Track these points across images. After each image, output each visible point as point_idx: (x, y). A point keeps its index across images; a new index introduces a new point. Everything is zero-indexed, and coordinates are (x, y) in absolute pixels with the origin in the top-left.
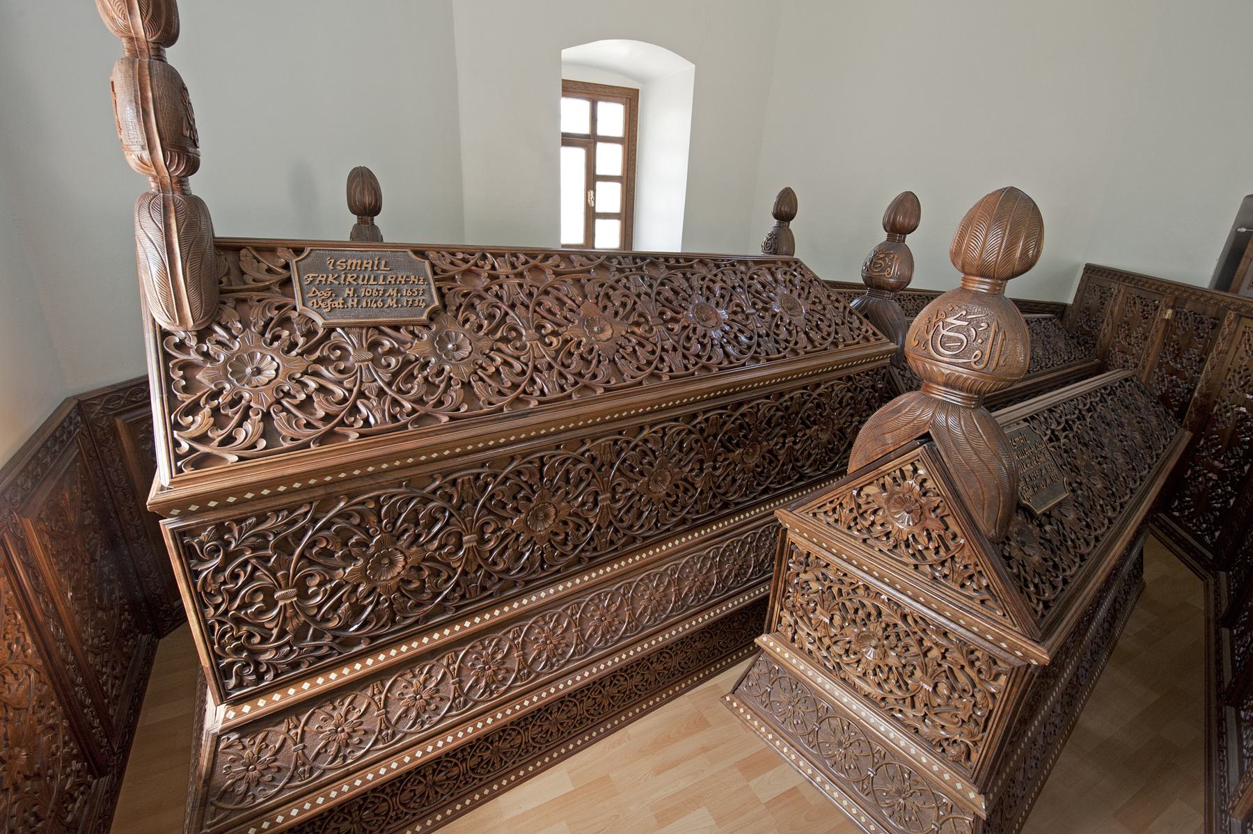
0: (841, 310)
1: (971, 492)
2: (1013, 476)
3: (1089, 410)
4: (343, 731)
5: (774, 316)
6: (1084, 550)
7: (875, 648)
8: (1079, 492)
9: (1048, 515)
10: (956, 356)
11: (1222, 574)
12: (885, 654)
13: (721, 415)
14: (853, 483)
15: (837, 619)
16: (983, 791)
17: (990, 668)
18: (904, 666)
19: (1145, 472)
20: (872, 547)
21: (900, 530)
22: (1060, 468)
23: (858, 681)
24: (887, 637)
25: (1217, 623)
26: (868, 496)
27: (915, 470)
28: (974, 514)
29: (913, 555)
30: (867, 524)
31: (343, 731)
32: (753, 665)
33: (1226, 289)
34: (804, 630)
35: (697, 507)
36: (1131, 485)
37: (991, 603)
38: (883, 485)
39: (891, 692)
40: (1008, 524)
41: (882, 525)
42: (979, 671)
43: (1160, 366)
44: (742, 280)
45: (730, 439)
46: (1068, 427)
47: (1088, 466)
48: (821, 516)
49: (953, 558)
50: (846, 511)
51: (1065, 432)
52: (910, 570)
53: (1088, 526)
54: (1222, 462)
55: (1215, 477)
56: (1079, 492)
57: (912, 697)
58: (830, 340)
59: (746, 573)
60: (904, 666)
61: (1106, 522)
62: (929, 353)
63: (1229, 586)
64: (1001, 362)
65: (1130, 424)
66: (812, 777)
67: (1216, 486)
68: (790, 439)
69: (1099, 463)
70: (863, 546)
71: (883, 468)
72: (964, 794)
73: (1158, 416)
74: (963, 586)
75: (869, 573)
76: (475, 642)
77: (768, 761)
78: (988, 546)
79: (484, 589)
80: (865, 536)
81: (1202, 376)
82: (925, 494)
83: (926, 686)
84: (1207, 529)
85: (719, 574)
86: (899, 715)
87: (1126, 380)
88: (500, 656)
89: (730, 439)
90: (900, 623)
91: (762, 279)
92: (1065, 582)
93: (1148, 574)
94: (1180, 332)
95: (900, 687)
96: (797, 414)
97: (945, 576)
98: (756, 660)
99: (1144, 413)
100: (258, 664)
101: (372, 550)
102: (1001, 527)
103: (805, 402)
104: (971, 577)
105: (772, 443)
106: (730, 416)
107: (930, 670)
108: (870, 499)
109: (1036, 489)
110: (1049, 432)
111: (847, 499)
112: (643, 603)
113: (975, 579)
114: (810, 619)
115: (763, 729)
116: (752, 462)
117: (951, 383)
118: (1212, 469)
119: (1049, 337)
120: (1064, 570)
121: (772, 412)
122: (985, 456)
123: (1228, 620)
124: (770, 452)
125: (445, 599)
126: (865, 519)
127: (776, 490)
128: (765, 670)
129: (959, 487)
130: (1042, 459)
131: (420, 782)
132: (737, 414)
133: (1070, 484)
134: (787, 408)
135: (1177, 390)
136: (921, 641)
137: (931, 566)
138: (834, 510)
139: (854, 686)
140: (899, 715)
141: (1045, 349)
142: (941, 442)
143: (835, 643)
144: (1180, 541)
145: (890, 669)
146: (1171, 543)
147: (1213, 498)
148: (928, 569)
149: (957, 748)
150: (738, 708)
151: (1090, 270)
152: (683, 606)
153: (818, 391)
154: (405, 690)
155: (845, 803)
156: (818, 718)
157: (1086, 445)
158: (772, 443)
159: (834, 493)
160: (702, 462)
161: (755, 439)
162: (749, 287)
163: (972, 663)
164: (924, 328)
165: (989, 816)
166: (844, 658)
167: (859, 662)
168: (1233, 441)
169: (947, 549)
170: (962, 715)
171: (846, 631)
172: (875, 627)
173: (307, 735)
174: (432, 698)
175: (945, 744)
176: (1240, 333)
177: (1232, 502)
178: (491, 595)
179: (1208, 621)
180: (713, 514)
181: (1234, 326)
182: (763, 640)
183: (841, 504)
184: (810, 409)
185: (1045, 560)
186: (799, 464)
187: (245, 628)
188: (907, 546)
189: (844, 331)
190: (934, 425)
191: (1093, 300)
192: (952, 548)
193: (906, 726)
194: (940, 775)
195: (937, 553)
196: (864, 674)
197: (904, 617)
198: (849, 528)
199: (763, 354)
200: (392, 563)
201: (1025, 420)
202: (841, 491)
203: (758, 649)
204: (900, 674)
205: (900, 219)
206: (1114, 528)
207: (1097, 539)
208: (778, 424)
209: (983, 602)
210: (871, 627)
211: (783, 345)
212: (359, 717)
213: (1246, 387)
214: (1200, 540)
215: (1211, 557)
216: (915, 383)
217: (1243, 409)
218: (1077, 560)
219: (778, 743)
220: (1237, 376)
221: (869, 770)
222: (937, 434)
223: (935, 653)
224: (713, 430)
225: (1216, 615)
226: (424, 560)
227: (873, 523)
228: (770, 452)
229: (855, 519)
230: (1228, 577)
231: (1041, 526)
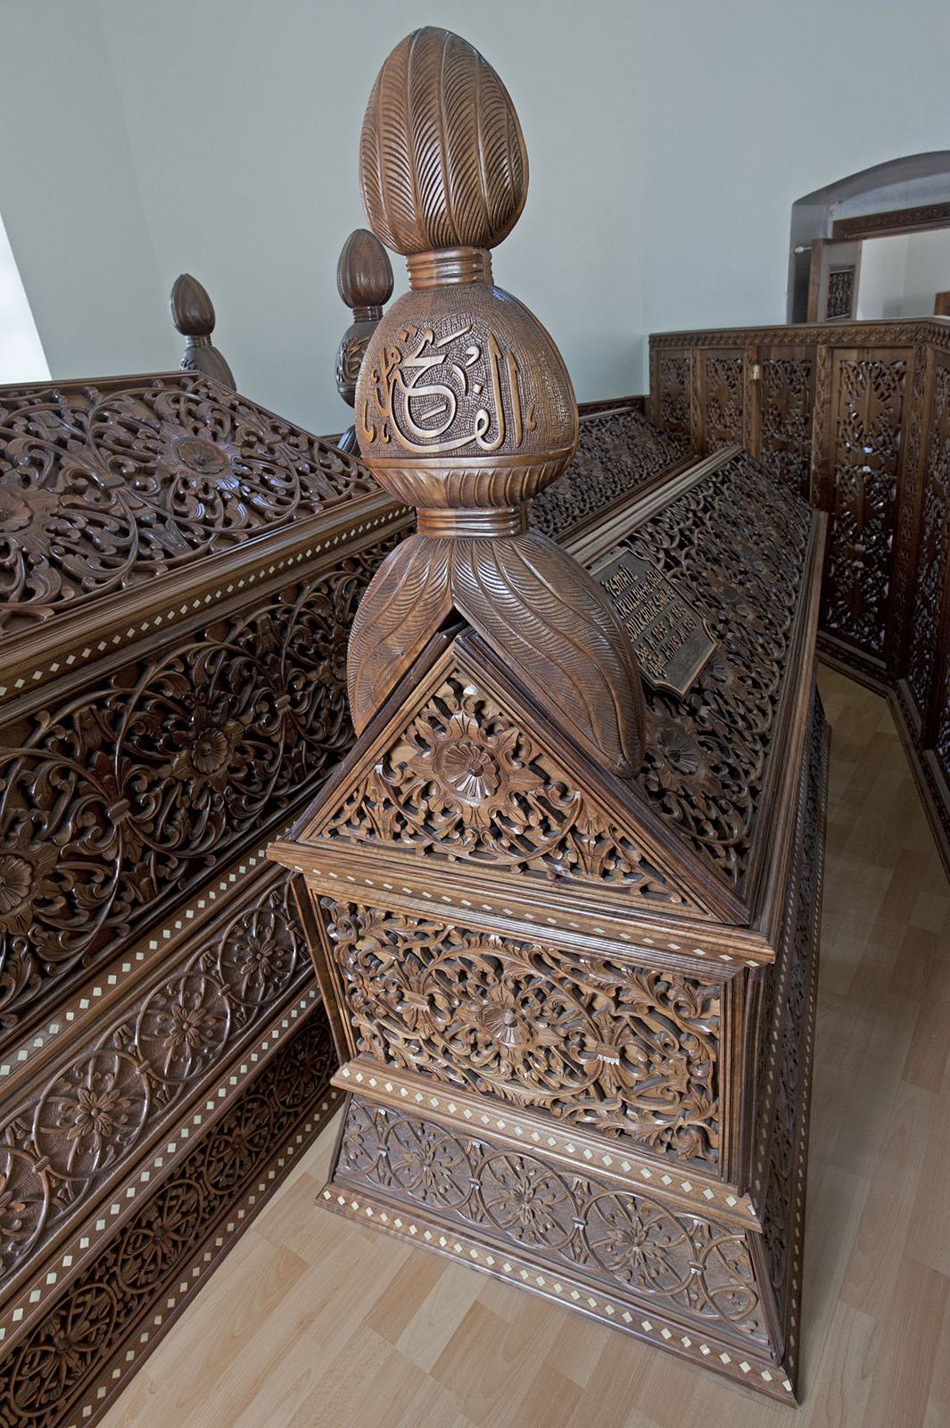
0: (304, 447)
1: (561, 699)
2: (620, 643)
3: (705, 510)
5: (168, 481)
6: (762, 726)
7: (513, 1025)
8: (729, 635)
9: (697, 690)
10: (445, 436)
11: (902, 682)
12: (532, 1032)
13: (100, 703)
14: (370, 753)
15: (441, 1002)
16: (744, 1189)
17: (691, 996)
18: (567, 1038)
19: (797, 579)
20: (444, 857)
21: (475, 812)
22: (692, 606)
23: (509, 1089)
24: (525, 1001)
25: (917, 747)
26: (402, 767)
27: (459, 690)
28: (578, 737)
29: (512, 848)
30: (419, 819)
32: (346, 1123)
33: (805, 321)
34: (398, 1037)
35: (130, 894)
36: (788, 603)
37: (657, 887)
38: (418, 737)
39: (562, 1086)
40: (640, 733)
41: (445, 811)
42: (678, 1007)
43: (766, 444)
44: (79, 425)
45: (148, 742)
46: (685, 542)
47: (729, 592)
48: (345, 831)
49: (573, 830)
50: (379, 807)
51: (684, 548)
52: (516, 876)
53: (756, 684)
54: (863, 543)
55: (860, 564)
56: (729, 635)
57: (596, 1084)
58: (296, 501)
59: (286, 964)
60: (567, 1038)
61: (776, 668)
62: (400, 447)
63: (914, 694)
64: (527, 421)
65: (760, 518)
66: (497, 1268)
67: (865, 575)
68: (281, 702)
69: (741, 583)
70: (429, 862)
71: (407, 706)
72: (718, 1203)
73: (785, 500)
74: (605, 873)
75: (456, 903)
77: (421, 1276)
78: (621, 788)
80: (427, 842)
81: (813, 441)
82: (490, 730)
83: (609, 1060)
84: (870, 633)
85: (232, 992)
86: (588, 1119)
87: (737, 459)
89: (148, 742)
90: (533, 972)
91: (126, 416)
92: (754, 792)
93: (831, 716)
94: (775, 393)
95: (572, 1074)
96: (277, 651)
97: (573, 867)
98: (347, 1113)
99: (770, 500)
102: (631, 746)
103: (284, 626)
104: (612, 854)
105: (247, 719)
106: (124, 698)
107: (605, 1032)
108: (408, 773)
109: (667, 652)
110: (661, 555)
111: (371, 787)
112: (73, 1137)
113: (619, 853)
114: (399, 1015)
115: (398, 1223)
116: (217, 767)
117: (461, 498)
118: (856, 556)
119: (632, 438)
120: (747, 773)
121: (221, 661)
122: (561, 622)
123: (928, 740)
124: (250, 735)
126: (415, 811)
127: (291, 797)
128: (366, 1123)
129: (539, 697)
130: (664, 600)
131: (146, 1237)
132: (140, 689)
133: (714, 628)
134: (251, 646)
135: (792, 468)
136: (576, 991)
137: (546, 857)
138: (361, 814)
139: (505, 1100)
140: (588, 1119)
141: (633, 455)
142: (481, 619)
143: (453, 1038)
144: (848, 658)
145: (548, 1050)
146: (838, 663)
147: (866, 592)
148: (543, 865)
149: (687, 1138)
150: (347, 1204)
151: (657, 341)
152: (172, 1090)
153: (302, 600)
155: (558, 1288)
156: (473, 1169)
157: (716, 561)
158: (247, 719)
159: (347, 782)
160: (98, 808)
161: (204, 724)
162: (100, 435)
163: (663, 998)
164: (373, 399)
165: (767, 1221)
166: (475, 1059)
167: (498, 1056)
168: (868, 514)
169: (560, 817)
170: (677, 1085)
171: (460, 1014)
172: (501, 992)
175: (667, 1138)
176: (837, 372)
177: (886, 588)
179: (907, 747)
180: (175, 890)
181: (828, 364)
182: (344, 1075)
183: (366, 799)
184: (299, 634)
185: (716, 769)
186: (319, 737)
188: (498, 834)
189: (319, 483)
190: (460, 593)
191: (671, 383)
192: (567, 812)
193: (603, 1132)
194: (675, 1188)
195: (547, 829)
196: (513, 1073)
197: (537, 959)
198: (397, 836)
199: (159, 557)
201: (622, 544)
202: (357, 773)
203: (343, 1094)
204: (564, 1054)
205: (362, 280)
206: (788, 674)
207: (773, 701)
208: (244, 682)
209: (644, 889)
210: (494, 993)
211: (199, 530)
213: (862, 440)
214: (866, 648)
215: (884, 665)
216: (401, 522)
217: (866, 469)
218: (758, 747)
219: (428, 1235)
220: (849, 429)
221: (573, 1223)
222: (469, 607)
223: (603, 1001)
224: (94, 738)
225: (913, 736)
227: (430, 815)
228: (250, 735)
229: (399, 817)
230: (910, 683)
231: (693, 712)
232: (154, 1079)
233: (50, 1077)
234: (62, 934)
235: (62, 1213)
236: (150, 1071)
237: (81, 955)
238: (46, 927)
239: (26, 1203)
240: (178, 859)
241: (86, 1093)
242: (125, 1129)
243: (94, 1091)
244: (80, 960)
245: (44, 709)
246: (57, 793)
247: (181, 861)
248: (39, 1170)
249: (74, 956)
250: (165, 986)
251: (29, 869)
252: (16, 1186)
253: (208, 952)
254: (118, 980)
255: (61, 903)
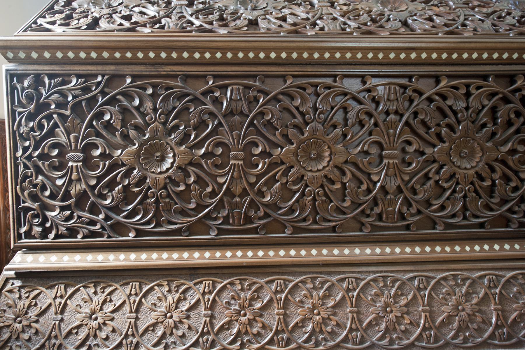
4: (463, 310)
31: (171, 317)
76: (235, 279)
79: (248, 220)
88: (259, 305)
100: (45, 219)
101: (458, 134)
125: (208, 216)
154: (160, 301)
173: (68, 310)
174: (181, 322)
178: (255, 231)
187: (40, 177)
200: (163, 159)
212: (113, 312)
226: (191, 164)
232: (501, 320)
233: (377, 272)
234: (482, 200)
235: (496, 342)
236: (500, 313)
237: (486, 219)
238: (476, 191)
239: (411, 322)
240: (265, 212)
241: (460, 294)
242: (474, 333)
243: (465, 296)
244: (485, 222)
245: (521, 74)
246: (510, 123)
247: (419, 212)
248: (351, 312)
249: (483, 217)
250: (458, 275)
251: (481, 154)
252: (410, 309)
253: (282, 282)
254: (263, 256)
255: (488, 183)
